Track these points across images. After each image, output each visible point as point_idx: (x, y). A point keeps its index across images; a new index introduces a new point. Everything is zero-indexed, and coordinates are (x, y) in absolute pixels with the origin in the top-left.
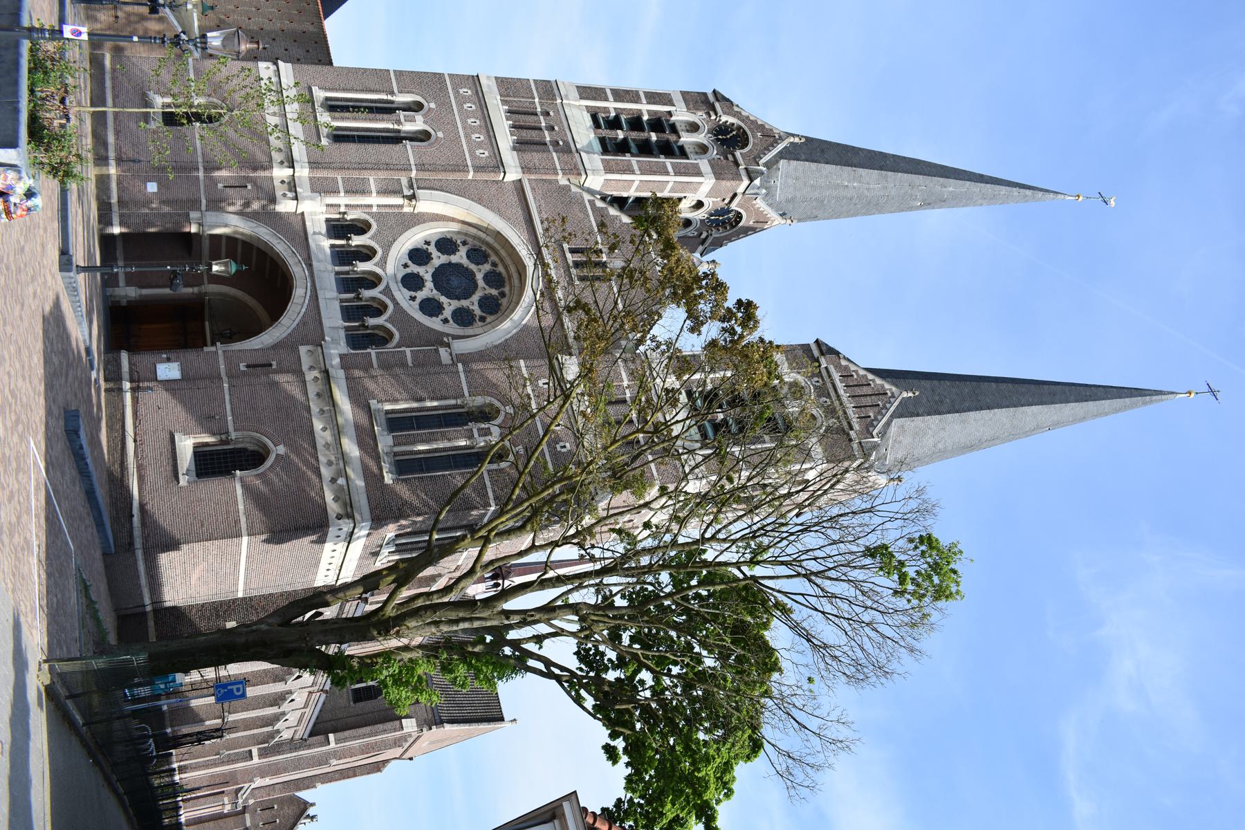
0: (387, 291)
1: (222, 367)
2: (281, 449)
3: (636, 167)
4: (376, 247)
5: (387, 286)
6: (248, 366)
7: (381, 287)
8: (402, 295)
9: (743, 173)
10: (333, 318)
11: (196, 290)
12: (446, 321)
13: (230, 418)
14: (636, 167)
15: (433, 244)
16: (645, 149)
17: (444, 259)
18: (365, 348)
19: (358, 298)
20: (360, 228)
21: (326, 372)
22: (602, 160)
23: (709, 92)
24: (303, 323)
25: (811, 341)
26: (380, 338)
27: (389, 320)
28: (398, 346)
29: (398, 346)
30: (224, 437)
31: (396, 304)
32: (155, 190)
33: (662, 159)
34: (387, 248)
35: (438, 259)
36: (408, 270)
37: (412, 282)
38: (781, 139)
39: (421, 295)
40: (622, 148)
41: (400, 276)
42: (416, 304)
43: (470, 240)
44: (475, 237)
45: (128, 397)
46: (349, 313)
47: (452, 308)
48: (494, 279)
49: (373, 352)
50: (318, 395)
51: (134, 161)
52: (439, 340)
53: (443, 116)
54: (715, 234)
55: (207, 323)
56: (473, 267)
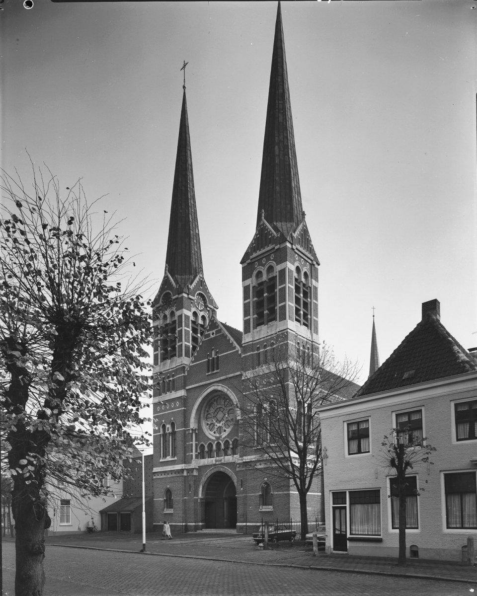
3: (180, 344)
9: (180, 296)
14: (180, 344)
16: (272, 300)
20: (202, 446)
25: (241, 266)
28: (238, 437)
29: (238, 437)
33: (277, 290)
38: (167, 276)
40: (272, 311)
43: (207, 409)
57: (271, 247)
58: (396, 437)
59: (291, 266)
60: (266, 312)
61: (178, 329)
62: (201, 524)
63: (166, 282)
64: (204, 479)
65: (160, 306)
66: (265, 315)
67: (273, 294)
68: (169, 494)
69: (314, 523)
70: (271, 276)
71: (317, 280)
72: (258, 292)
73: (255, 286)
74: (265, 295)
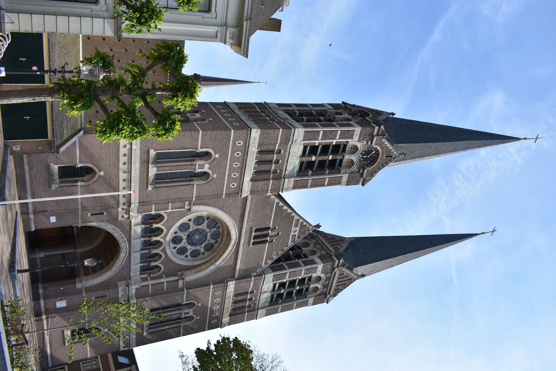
0: (164, 250)
5: (164, 248)
32: (54, 217)
34: (168, 229)
45: (45, 322)
46: (144, 258)
48: (215, 236)
49: (153, 212)
51: (43, 212)
53: (219, 166)
57: (331, 249)
58: (132, 282)
59: (319, 269)
61: (300, 261)
63: (342, 239)
64: (109, 228)
67: (293, 258)
71: (314, 303)
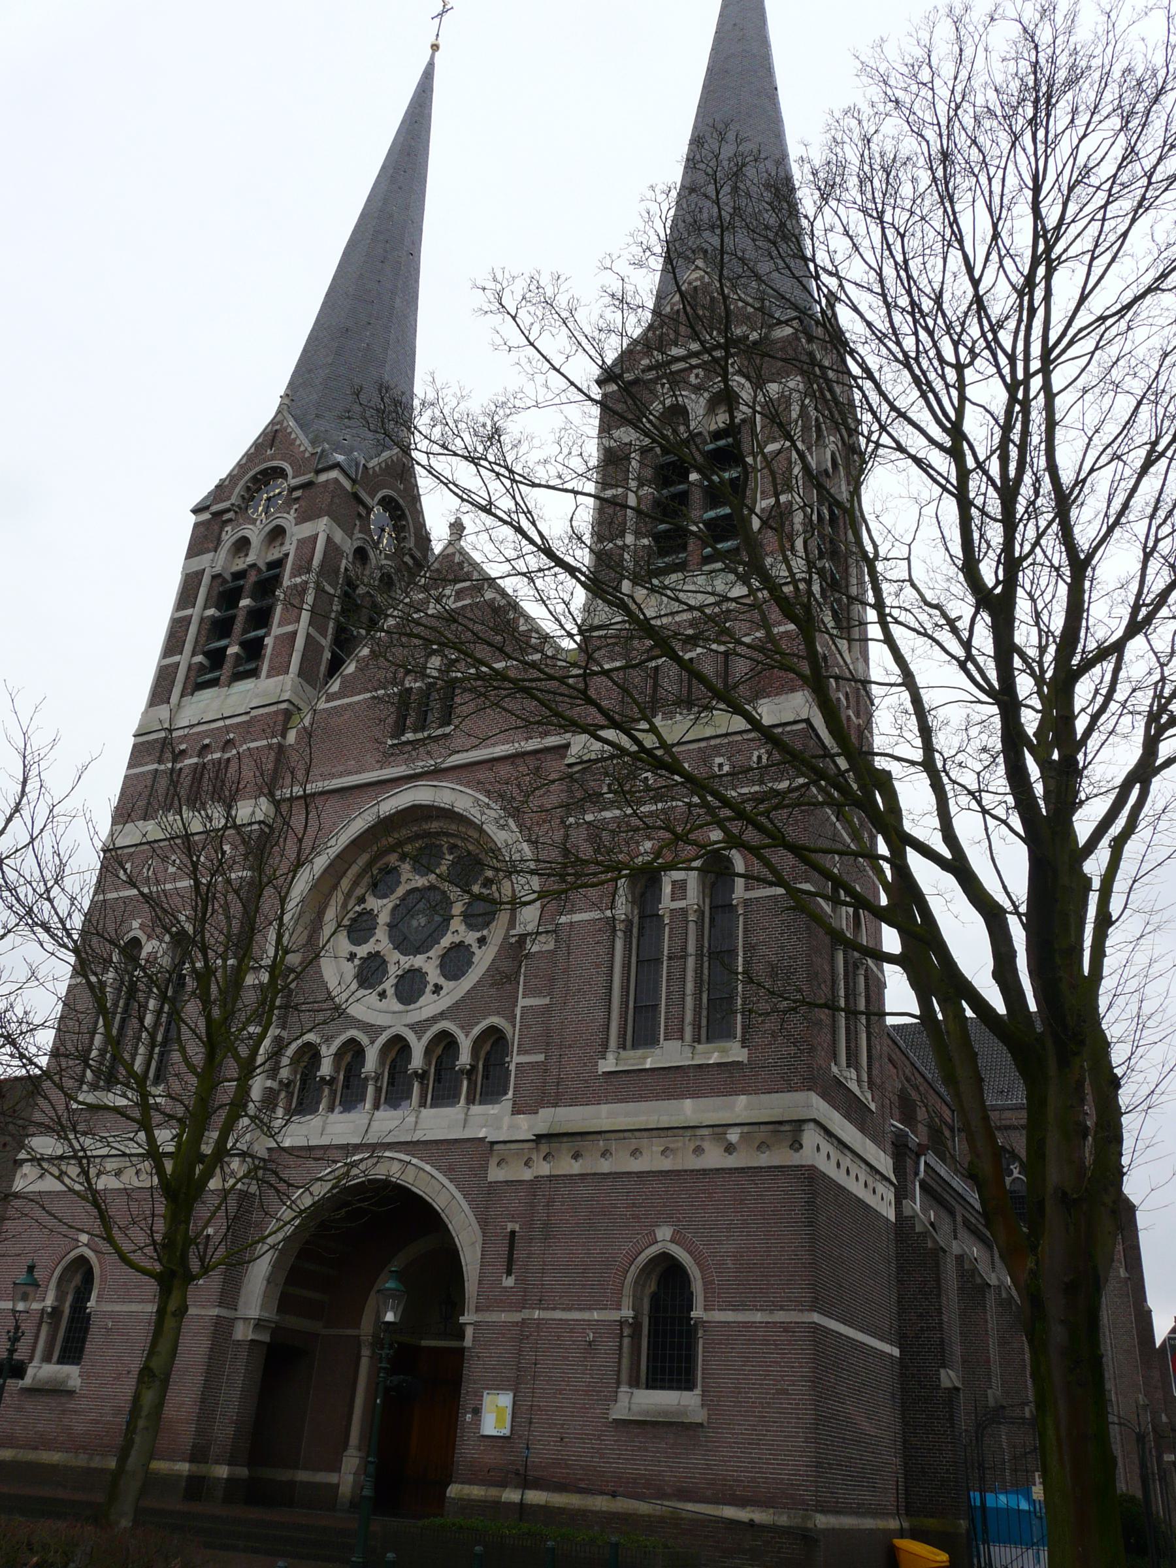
0: (419, 1028)
1: (503, 1317)
2: (664, 1233)
3: (290, 628)
4: (343, 1038)
5: (411, 1027)
6: (509, 1273)
7: (411, 1037)
8: (428, 1006)
10: (441, 1122)
11: (366, 1352)
12: (482, 941)
13: (596, 1315)
15: (355, 949)
17: (381, 934)
18: (508, 1071)
19: (422, 1076)
21: (539, 1138)
22: (268, 676)
23: (192, 519)
24: (449, 1171)
26: (493, 1043)
27: (466, 1030)
28: (511, 1019)
29: (511, 1019)
30: (626, 1332)
31: (442, 1015)
35: (381, 941)
36: (390, 992)
37: (410, 987)
39: (434, 975)
41: (398, 1007)
42: (447, 985)
43: (359, 891)
44: (355, 883)
47: (462, 928)
49: (516, 1059)
50: (576, 1156)
52: (516, 949)
54: (411, 543)
55: (424, 1343)
56: (401, 891)
60: (233, 650)
62: (223, 1471)
65: (227, 511)
66: (228, 659)
68: (77, 1280)
69: (184, 1467)
70: (275, 554)
72: (227, 593)
73: (219, 575)
74: (245, 602)
